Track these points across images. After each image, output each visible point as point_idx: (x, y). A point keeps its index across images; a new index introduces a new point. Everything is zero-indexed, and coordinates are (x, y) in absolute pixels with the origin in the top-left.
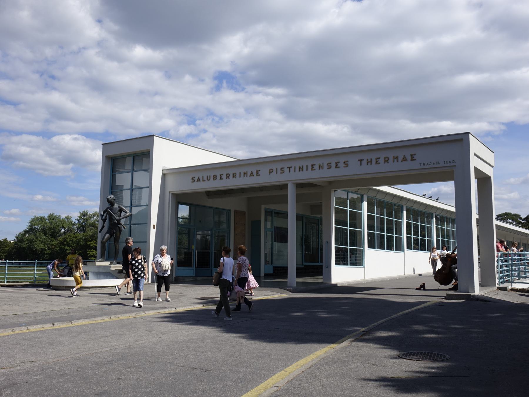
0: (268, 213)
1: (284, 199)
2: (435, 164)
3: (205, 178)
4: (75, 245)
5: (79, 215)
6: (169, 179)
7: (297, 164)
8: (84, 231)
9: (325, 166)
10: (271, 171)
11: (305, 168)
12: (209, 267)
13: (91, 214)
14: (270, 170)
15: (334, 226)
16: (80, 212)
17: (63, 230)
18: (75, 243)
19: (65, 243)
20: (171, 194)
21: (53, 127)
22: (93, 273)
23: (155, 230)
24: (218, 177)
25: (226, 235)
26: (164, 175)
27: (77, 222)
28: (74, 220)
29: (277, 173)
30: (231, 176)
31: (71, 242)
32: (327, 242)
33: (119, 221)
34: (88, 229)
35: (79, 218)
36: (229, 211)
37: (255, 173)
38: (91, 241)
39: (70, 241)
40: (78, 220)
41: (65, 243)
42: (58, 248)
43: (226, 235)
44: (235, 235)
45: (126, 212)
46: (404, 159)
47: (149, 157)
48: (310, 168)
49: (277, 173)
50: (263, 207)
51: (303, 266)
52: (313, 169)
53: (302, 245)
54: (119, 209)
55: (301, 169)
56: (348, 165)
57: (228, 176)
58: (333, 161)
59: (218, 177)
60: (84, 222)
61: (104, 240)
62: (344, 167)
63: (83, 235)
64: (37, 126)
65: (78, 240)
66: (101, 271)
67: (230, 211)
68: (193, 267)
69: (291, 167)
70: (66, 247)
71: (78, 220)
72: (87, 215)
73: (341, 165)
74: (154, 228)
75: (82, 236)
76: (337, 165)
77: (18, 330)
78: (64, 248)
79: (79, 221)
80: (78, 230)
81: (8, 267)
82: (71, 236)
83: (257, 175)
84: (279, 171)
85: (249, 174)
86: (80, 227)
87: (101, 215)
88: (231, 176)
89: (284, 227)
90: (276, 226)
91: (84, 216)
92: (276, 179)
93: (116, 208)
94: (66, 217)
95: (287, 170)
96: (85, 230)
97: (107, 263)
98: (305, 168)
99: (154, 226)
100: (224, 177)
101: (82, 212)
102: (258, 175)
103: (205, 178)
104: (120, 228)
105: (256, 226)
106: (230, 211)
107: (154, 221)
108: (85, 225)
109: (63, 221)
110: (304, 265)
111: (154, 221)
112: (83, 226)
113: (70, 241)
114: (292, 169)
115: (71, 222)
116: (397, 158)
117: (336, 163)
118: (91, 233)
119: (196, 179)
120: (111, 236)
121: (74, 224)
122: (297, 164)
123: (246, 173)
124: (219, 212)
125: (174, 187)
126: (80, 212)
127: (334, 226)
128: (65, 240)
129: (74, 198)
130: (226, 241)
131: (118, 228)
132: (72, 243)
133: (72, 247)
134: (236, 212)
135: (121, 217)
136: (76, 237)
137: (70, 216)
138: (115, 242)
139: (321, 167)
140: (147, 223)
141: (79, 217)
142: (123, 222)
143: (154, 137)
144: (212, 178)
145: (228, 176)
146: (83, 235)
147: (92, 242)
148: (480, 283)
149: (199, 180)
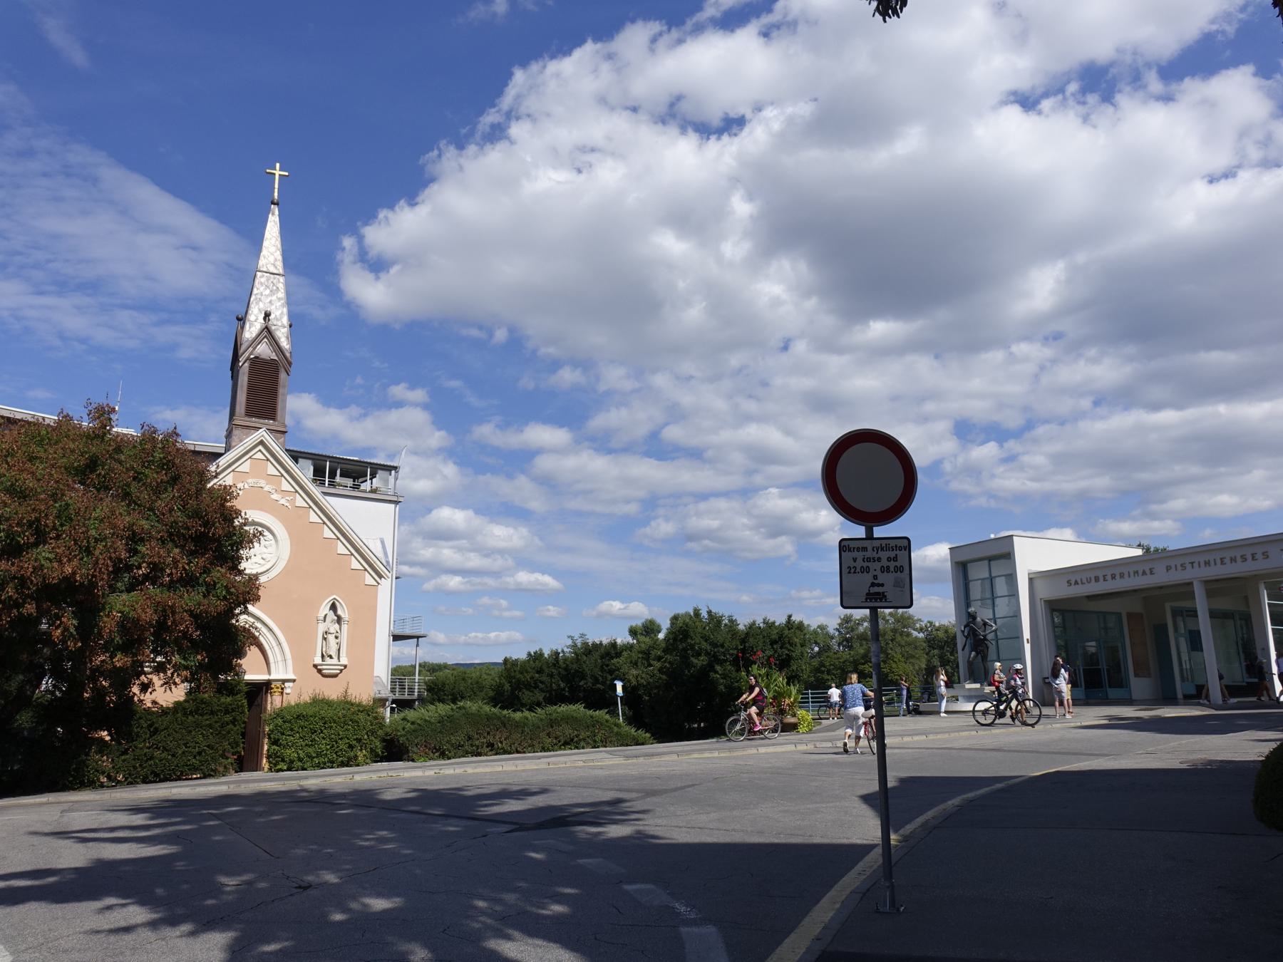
0: (1176, 613)
1: (1191, 595)
2: (1078, 584)
3: (1085, 581)
4: (839, 671)
5: (839, 621)
6: (1037, 584)
7: (1202, 559)
8: (851, 648)
9: (1239, 559)
10: (1168, 568)
11: (1212, 563)
12: (1102, 687)
13: (858, 618)
14: (1167, 567)
15: (1270, 627)
16: (840, 617)
17: (816, 649)
18: (839, 669)
19: (823, 669)
20: (1042, 601)
21: (758, 479)
22: (964, 696)
23: (1029, 645)
24: (1101, 579)
25: (1119, 645)
26: (1031, 580)
27: (837, 633)
28: (831, 630)
29: (1176, 570)
30: (1118, 577)
31: (832, 667)
32: (1263, 649)
33: (985, 636)
34: (856, 645)
35: (840, 626)
36: (1119, 615)
37: (1148, 572)
38: (864, 664)
39: (831, 665)
40: (837, 629)
41: (823, 669)
42: (813, 678)
43: (1119, 645)
44: (1132, 644)
45: (992, 626)
46: (1144, 573)
47: (1010, 558)
48: (1219, 561)
49: (1176, 570)
50: (1168, 606)
51: (1244, 684)
52: (1222, 563)
53: (1239, 653)
54: (982, 623)
55: (1207, 563)
56: (1268, 557)
57: (1113, 577)
58: (1248, 553)
59: (1101, 579)
60: (848, 633)
61: (971, 659)
62: (1264, 558)
63: (850, 654)
64: (736, 481)
65: (844, 662)
66: (973, 694)
67: (1120, 614)
68: (1081, 687)
69: (1194, 562)
70: (826, 677)
71: (837, 629)
72: (851, 621)
73: (1259, 556)
74: (1028, 642)
75: (848, 656)
76: (1104, 578)
77: (939, 736)
78: (823, 678)
79: (839, 631)
80: (839, 646)
81: (812, 698)
82: (831, 658)
83: (1152, 573)
84: (1179, 567)
85: (1140, 573)
86: (843, 641)
87: (962, 631)
88: (1118, 577)
89: (1196, 629)
90: (1190, 628)
91: (847, 622)
92: (1177, 577)
93: (979, 622)
94: (819, 627)
95: (1189, 566)
96: (852, 646)
97: (978, 686)
98: (1212, 563)
99: (1028, 640)
100: (1109, 577)
101: (842, 617)
102: (1152, 573)
103: (1085, 581)
104: (987, 645)
105: (1160, 633)
106: (1120, 614)
107: (1027, 634)
108: (851, 638)
109: (815, 632)
110: (1247, 683)
111: (1027, 634)
112: (847, 640)
113: (831, 665)
114: (1196, 565)
115: (827, 634)
116: (1137, 572)
117: (1252, 555)
118: (862, 651)
119: (1073, 582)
120: (978, 653)
121: (832, 638)
122: (1202, 559)
123: (1136, 573)
124: (1105, 614)
125: (1045, 593)
126: (840, 617)
127: (1270, 627)
128: (822, 664)
129: (805, 594)
130: (1121, 653)
131: (985, 646)
132: (833, 669)
133: (834, 675)
134: (1130, 615)
135: (987, 632)
136: (838, 658)
137: (825, 624)
138: (982, 661)
139: (1233, 560)
140: (1018, 637)
141: (839, 625)
142: (990, 637)
143: (1014, 537)
144: (1093, 579)
145: (1113, 577)
146: (850, 654)
147: (866, 666)
148: (1061, 642)
149: (1076, 583)
